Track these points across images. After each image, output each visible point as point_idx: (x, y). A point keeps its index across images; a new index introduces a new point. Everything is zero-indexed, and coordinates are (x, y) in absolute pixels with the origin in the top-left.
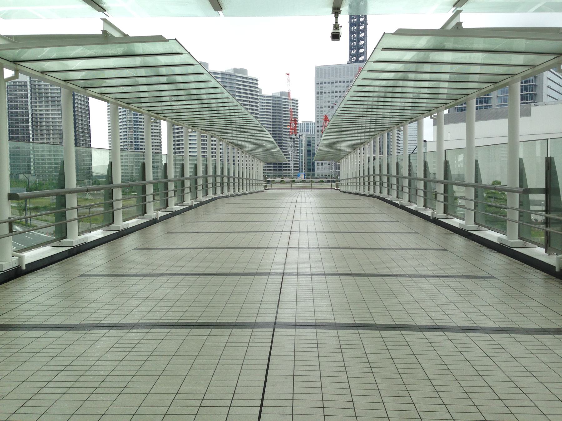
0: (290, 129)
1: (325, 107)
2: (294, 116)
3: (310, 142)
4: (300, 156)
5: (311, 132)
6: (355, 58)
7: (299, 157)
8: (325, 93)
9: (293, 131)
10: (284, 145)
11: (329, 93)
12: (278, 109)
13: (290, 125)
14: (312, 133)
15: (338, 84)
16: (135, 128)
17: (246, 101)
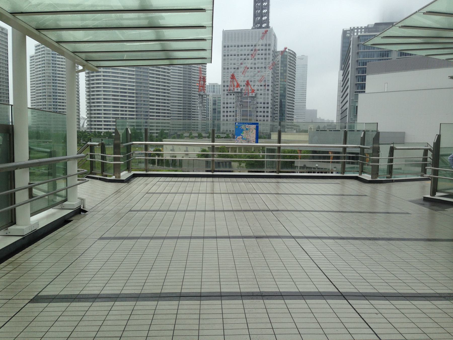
0: (199, 86)
1: (231, 68)
2: (203, 75)
3: (216, 102)
4: (206, 113)
5: (216, 93)
6: (259, 25)
7: (206, 114)
8: (231, 55)
9: (202, 88)
10: (193, 89)
11: (235, 55)
13: (199, 82)
14: (217, 94)
15: (243, 48)
16: (53, 83)
17: (159, 106)
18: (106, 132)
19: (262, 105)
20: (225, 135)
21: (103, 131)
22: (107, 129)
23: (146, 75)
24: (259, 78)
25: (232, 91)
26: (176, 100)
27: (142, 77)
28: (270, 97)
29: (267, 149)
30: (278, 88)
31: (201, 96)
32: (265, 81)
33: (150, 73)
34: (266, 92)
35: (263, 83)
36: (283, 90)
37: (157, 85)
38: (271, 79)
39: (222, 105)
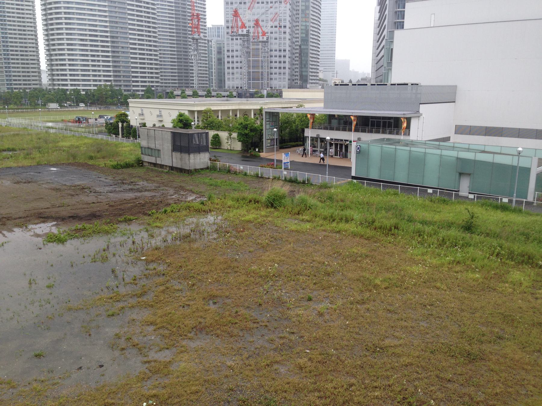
9: (196, 30)
12: (184, 50)
13: (191, 22)
17: (144, 54)
18: (74, 90)
19: (278, 53)
20: (228, 93)
21: (69, 88)
22: (75, 85)
23: (124, 11)
24: (271, 17)
25: (235, 34)
26: (168, 47)
27: (117, 15)
28: (288, 42)
29: (266, 112)
30: (298, 30)
31: (195, 40)
32: (280, 20)
33: (129, 9)
34: (283, 36)
35: (276, 23)
36: (304, 33)
37: (138, 25)
38: (288, 19)
39: (226, 53)
